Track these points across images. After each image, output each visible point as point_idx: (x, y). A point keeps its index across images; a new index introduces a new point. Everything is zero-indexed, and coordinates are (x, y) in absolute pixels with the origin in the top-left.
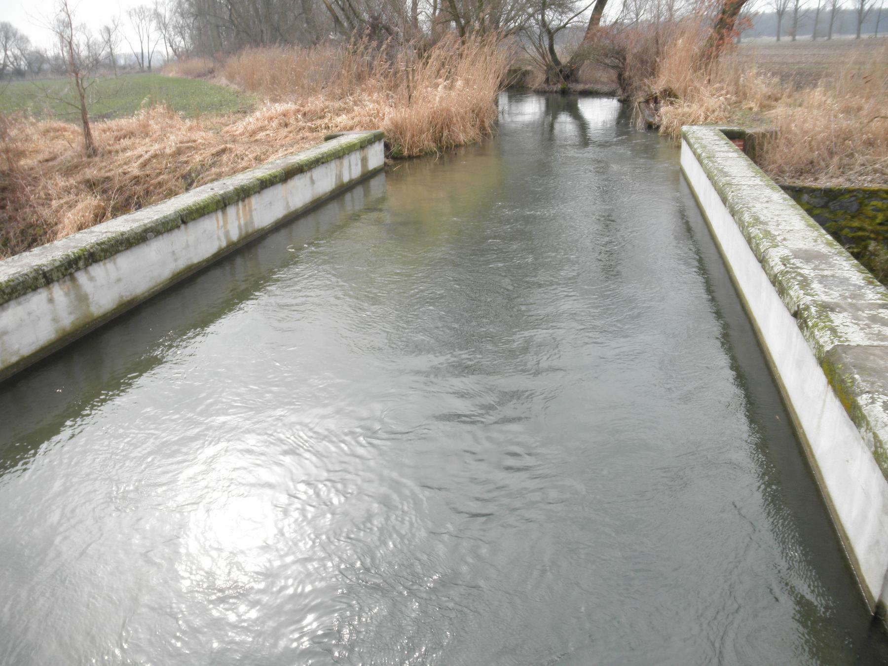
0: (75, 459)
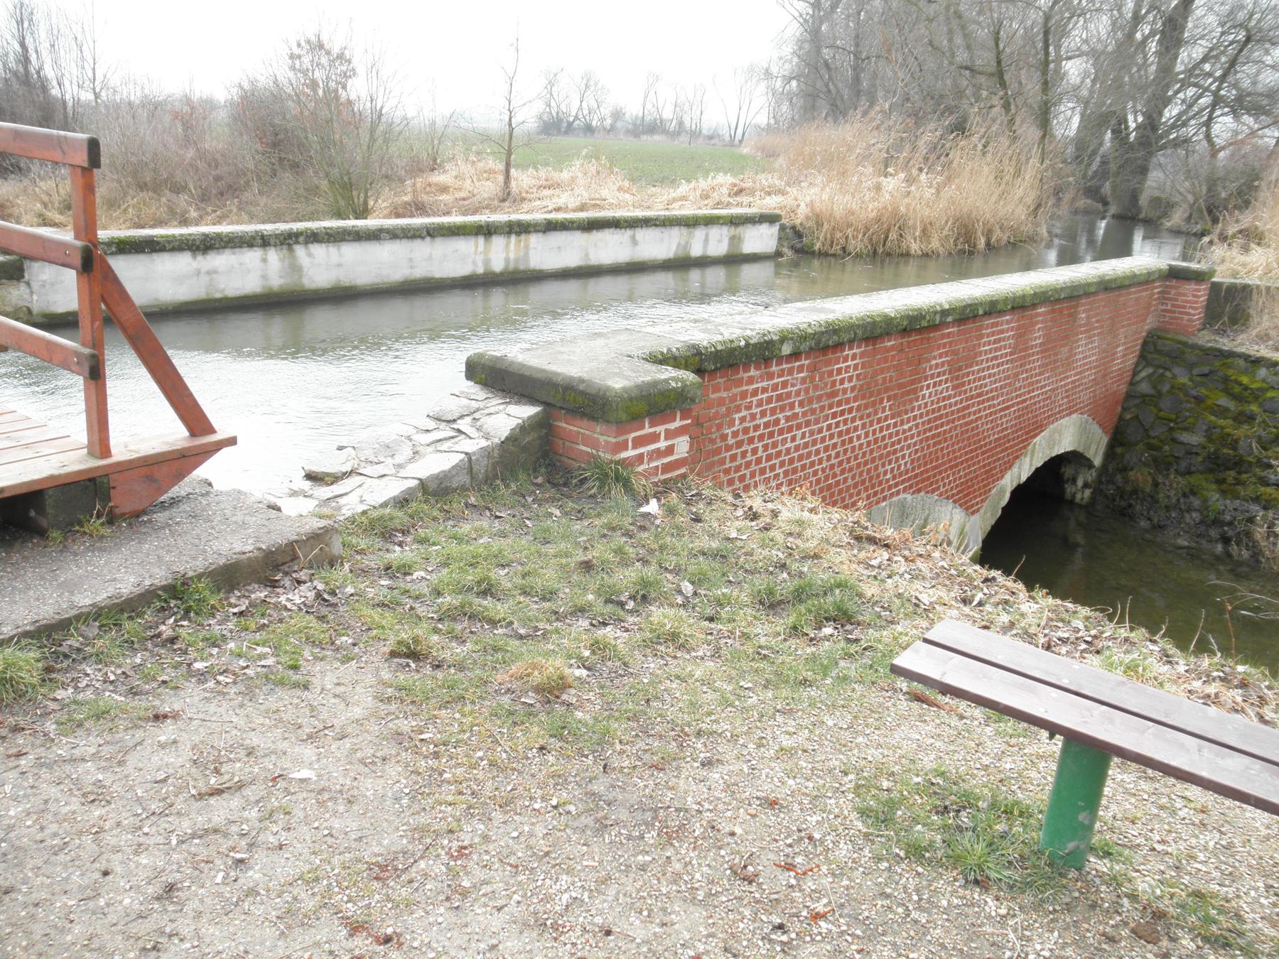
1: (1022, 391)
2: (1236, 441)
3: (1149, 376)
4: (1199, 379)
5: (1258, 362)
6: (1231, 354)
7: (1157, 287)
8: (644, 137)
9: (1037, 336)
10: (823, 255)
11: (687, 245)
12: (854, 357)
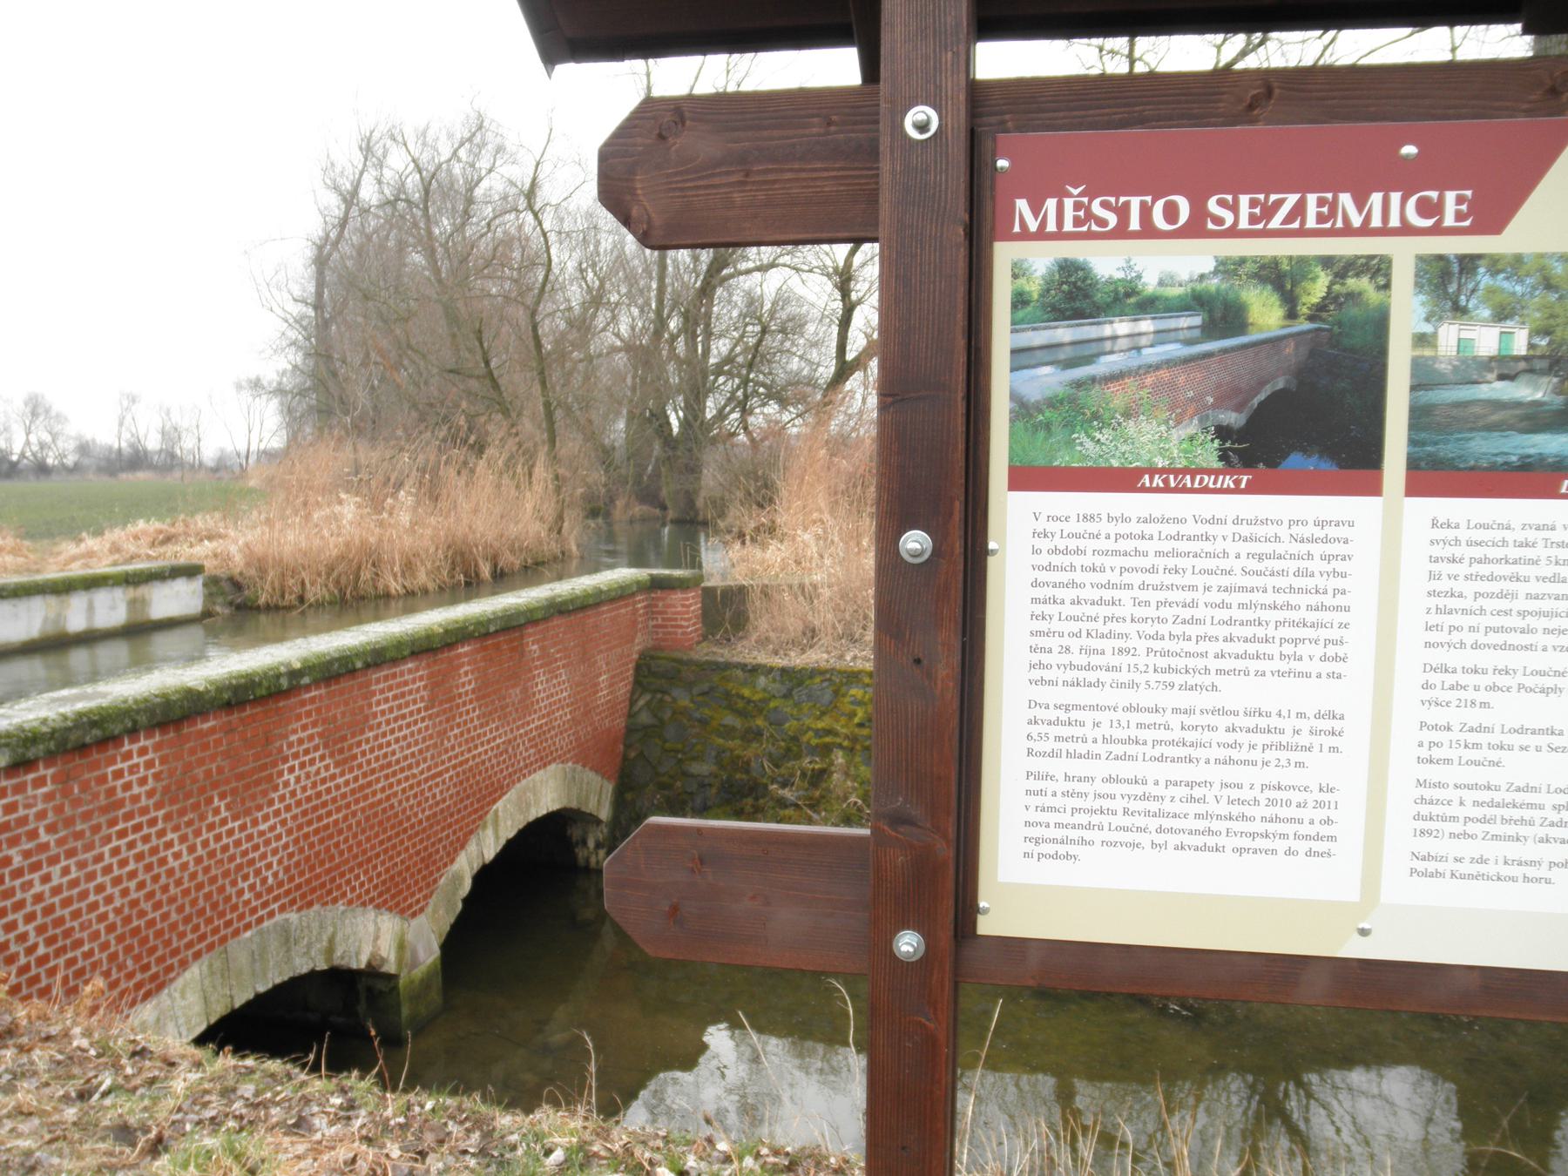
0: (950, 830)
1: (457, 750)
2: (748, 763)
3: (648, 704)
4: (700, 699)
5: (755, 670)
6: (728, 666)
7: (639, 601)
8: (124, 476)
9: (466, 681)
10: (269, 608)
11: (60, 617)
12: (143, 751)
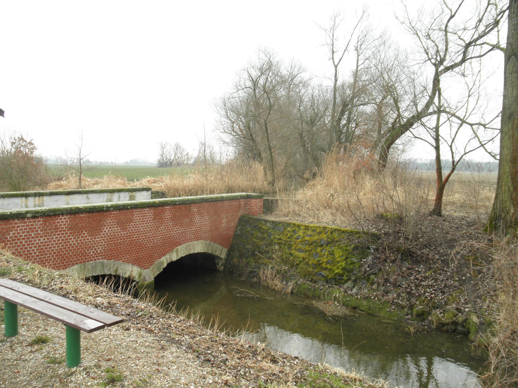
3: (240, 229)
